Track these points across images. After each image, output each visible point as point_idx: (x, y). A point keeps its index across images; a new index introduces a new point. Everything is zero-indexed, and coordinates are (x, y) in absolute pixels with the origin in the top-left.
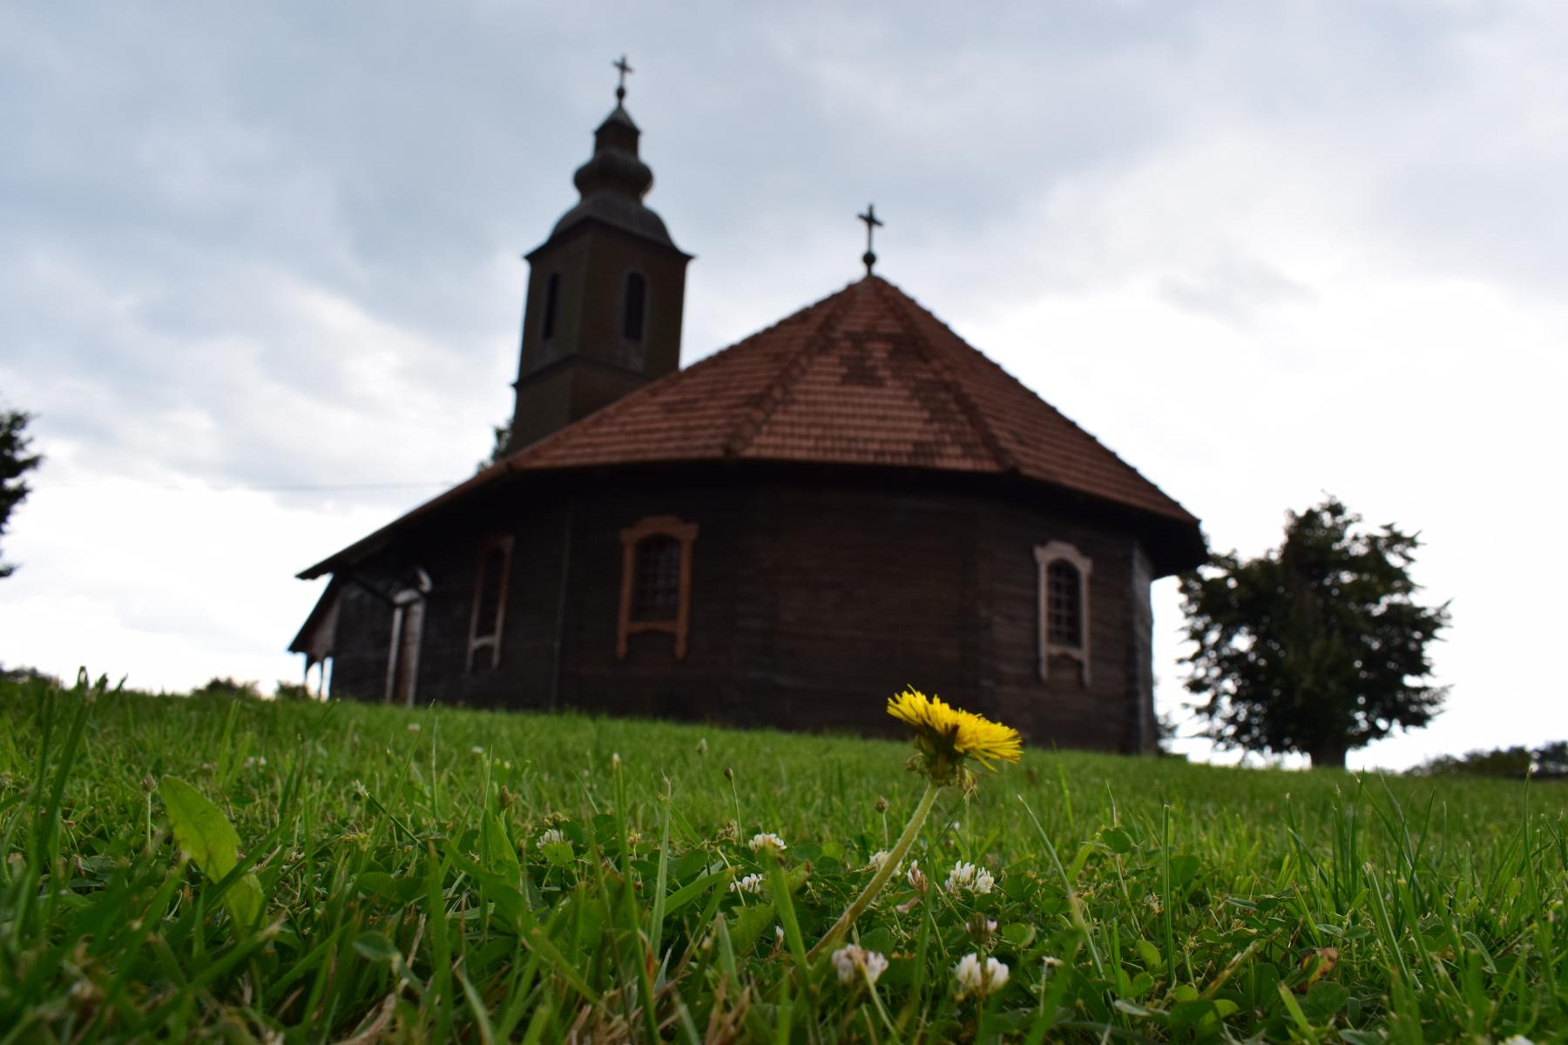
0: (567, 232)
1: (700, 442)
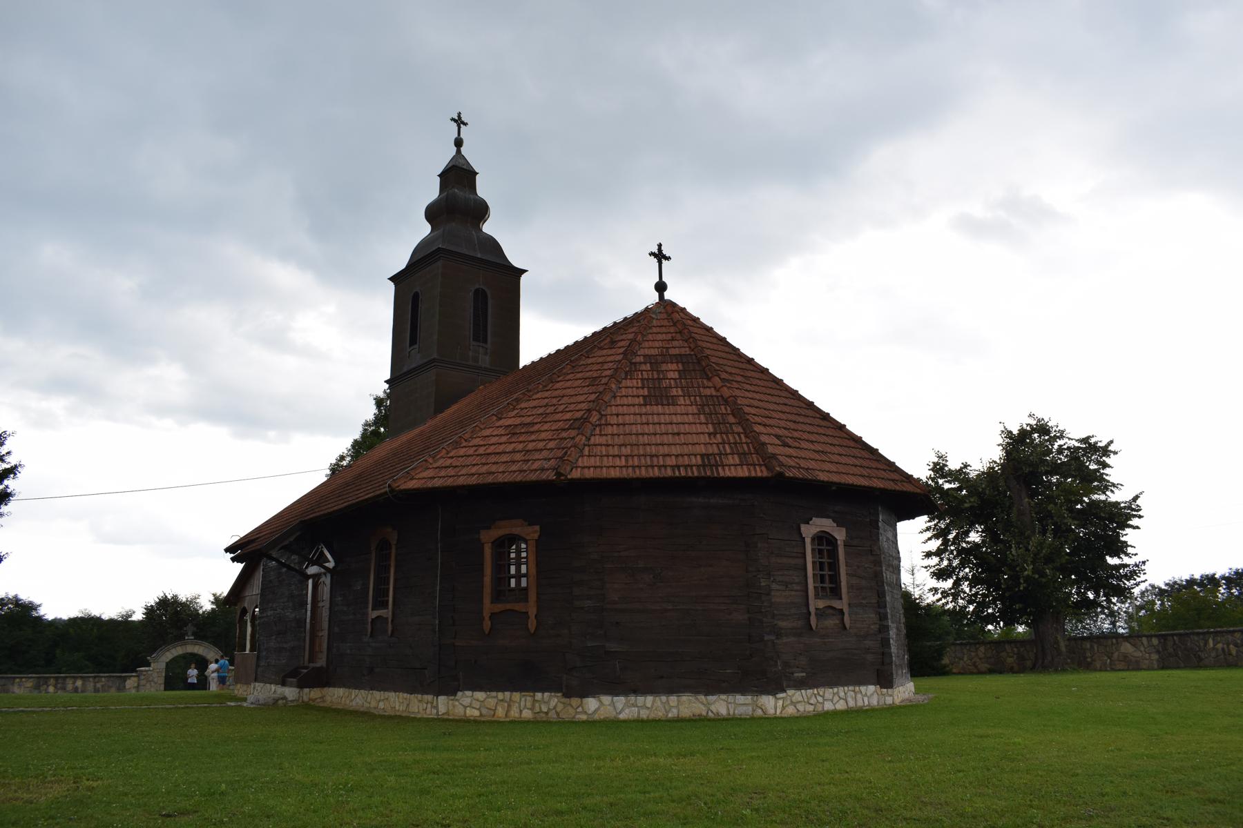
0: (422, 258)
1: (536, 465)
